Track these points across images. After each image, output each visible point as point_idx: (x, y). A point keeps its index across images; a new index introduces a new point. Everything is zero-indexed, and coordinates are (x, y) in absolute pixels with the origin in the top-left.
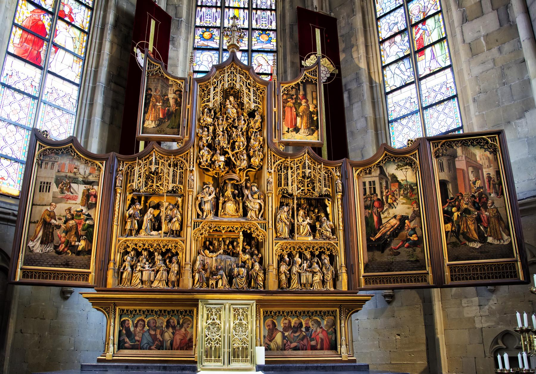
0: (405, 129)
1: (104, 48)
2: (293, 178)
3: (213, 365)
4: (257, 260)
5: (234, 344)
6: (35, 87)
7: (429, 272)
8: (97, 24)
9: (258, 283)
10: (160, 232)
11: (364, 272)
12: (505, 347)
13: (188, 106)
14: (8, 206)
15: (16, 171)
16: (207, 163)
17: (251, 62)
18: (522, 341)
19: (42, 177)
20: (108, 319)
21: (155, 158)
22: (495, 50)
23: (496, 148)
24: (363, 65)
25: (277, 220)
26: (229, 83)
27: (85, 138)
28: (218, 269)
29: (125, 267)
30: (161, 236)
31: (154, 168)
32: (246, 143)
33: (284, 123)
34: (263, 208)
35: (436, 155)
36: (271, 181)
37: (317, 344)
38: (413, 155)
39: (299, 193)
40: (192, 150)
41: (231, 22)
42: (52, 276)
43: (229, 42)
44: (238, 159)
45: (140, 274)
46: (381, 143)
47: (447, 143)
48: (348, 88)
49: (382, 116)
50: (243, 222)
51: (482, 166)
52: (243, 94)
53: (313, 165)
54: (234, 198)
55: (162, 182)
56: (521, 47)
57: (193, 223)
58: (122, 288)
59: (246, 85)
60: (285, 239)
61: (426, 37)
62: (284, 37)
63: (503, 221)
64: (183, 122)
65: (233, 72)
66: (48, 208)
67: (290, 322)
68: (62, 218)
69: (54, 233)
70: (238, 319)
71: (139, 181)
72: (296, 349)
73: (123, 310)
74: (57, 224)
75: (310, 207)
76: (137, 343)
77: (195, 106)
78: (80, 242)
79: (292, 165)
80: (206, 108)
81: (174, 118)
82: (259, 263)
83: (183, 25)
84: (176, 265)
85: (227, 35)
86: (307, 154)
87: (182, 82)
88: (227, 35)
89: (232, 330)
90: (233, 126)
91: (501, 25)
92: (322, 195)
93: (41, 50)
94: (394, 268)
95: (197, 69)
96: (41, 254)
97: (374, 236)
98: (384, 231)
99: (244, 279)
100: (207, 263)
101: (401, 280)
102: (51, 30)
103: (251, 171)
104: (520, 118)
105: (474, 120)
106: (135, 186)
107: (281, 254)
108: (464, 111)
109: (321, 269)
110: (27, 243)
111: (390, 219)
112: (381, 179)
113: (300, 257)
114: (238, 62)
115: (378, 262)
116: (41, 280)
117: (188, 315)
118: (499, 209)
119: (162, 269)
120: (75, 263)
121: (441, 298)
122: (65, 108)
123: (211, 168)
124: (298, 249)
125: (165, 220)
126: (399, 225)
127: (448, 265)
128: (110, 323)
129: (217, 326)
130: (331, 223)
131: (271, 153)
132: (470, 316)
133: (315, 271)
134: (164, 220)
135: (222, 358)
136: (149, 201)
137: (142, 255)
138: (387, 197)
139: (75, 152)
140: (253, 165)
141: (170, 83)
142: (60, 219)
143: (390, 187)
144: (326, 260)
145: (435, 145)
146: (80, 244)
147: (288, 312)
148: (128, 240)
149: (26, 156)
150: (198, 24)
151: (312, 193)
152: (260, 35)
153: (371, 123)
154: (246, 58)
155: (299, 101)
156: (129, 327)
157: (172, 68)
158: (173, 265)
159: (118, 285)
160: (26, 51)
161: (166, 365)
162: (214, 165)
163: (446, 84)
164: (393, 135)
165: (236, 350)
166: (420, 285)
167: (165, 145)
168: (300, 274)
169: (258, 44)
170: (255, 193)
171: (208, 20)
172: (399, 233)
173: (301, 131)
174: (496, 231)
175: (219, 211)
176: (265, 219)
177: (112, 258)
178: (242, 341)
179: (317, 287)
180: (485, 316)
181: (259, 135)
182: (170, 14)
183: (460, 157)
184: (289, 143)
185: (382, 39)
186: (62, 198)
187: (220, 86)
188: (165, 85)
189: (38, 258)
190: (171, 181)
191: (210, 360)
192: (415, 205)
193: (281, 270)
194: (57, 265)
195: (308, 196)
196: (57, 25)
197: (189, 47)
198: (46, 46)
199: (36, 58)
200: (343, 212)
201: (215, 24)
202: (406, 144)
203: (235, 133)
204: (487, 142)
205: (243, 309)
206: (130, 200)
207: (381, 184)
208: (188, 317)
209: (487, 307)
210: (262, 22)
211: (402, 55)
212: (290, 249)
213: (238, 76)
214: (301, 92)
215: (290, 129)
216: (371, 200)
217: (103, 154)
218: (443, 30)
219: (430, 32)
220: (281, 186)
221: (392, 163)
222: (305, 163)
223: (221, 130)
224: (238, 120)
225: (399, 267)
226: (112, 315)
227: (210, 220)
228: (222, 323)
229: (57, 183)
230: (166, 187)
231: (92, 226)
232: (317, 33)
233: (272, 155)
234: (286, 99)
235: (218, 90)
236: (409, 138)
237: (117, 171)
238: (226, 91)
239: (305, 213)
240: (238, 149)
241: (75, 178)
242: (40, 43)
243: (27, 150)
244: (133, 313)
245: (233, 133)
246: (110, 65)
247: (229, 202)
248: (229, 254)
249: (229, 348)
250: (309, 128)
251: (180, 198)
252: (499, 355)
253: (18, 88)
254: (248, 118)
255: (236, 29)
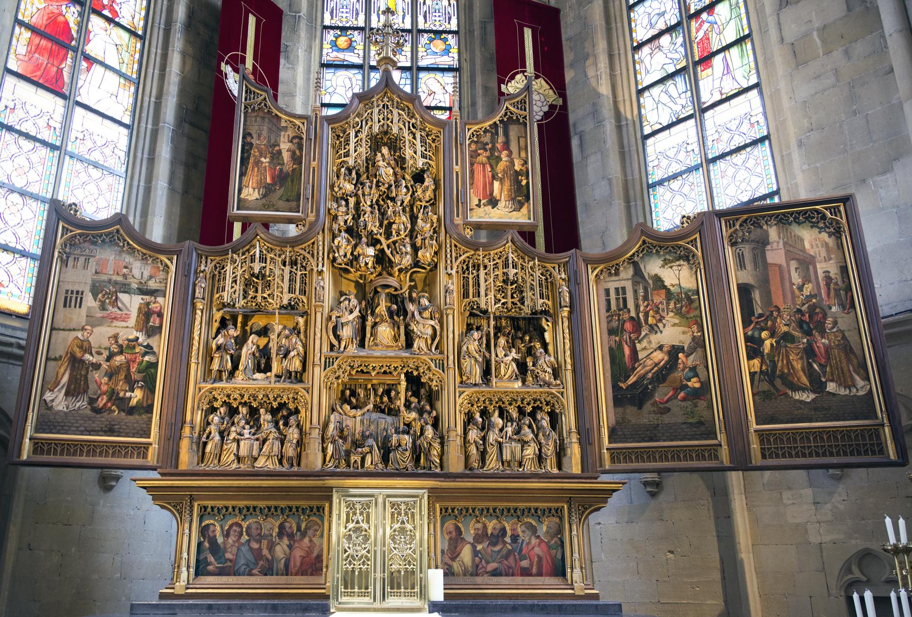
0: (678, 196)
1: (171, 63)
2: (487, 283)
3: (357, 601)
4: (430, 421)
5: (391, 565)
6: (55, 129)
7: (723, 443)
8: (158, 22)
9: (432, 459)
10: (269, 374)
11: (610, 442)
12: (865, 579)
13: (314, 164)
14: (9, 332)
15: (24, 271)
16: (345, 260)
17: (417, 89)
18: (898, 569)
19: (69, 282)
20: (179, 523)
21: (260, 251)
22: (838, 54)
23: (841, 227)
24: (604, 89)
25: (462, 354)
26: (381, 123)
27: (141, 217)
28: (364, 437)
29: (210, 433)
30: (270, 382)
31: (259, 268)
32: (409, 226)
33: (472, 190)
34: (438, 333)
35: (731, 240)
36: (451, 288)
37: (531, 564)
38: (692, 241)
39: (498, 309)
40: (320, 237)
41: (382, 18)
42: (85, 450)
43: (379, 54)
44: (397, 253)
45: (235, 445)
46: (635, 222)
47: (751, 220)
48: (578, 131)
49: (637, 176)
50: (406, 358)
51: (814, 258)
52: (405, 142)
53: (521, 261)
54: (391, 317)
55: (272, 290)
56: (886, 47)
57: (323, 360)
58: (204, 470)
59: (409, 127)
60: (475, 385)
61: (714, 35)
62: (470, 43)
63: (854, 354)
64: (306, 190)
65: (387, 105)
66: (79, 334)
67: (485, 527)
68: (103, 351)
69: (89, 376)
70: (398, 521)
71: (233, 290)
72: (495, 573)
73: (205, 508)
74: (94, 361)
75: (516, 332)
76: (229, 564)
77: (324, 163)
78: (133, 392)
79: (486, 261)
80: (343, 167)
81: (290, 184)
82: (433, 425)
83: (303, 25)
84: (296, 431)
85: (376, 41)
86: (510, 244)
87: (303, 123)
88: (376, 41)
89: (388, 540)
90: (388, 197)
91: (849, 9)
92: (536, 311)
93: (63, 66)
94: (660, 435)
95: (326, 100)
96: (65, 413)
97: (626, 381)
98: (642, 372)
99: (407, 453)
100: (347, 426)
101: (673, 457)
102: (79, 31)
103: (419, 272)
104: (885, 172)
105: (800, 179)
106: (226, 298)
107: (469, 411)
108: (781, 164)
109: (537, 436)
110: (42, 394)
111: (652, 352)
112: (635, 283)
113: (501, 416)
114: (396, 89)
115: (633, 425)
116: (65, 457)
117: (315, 514)
118: (847, 334)
119: (271, 437)
120: (125, 427)
121: (745, 488)
122: (106, 164)
123: (352, 267)
124: (497, 403)
125: (277, 354)
126: (667, 363)
127: (755, 431)
128: (183, 530)
129: (364, 533)
130: (552, 359)
131: (451, 242)
132: (798, 521)
133: (526, 439)
134: (275, 355)
135: (371, 589)
136: (250, 324)
137: (239, 413)
138: (646, 315)
139: (125, 240)
140: (422, 262)
141: (283, 124)
142: (99, 353)
143: (652, 296)
144: (544, 421)
145: (730, 224)
146: (133, 395)
147: (482, 509)
148: (215, 389)
149: (41, 246)
150: (327, 22)
151: (520, 309)
152: (431, 40)
153: (618, 189)
154: (409, 82)
155: (496, 154)
156: (215, 536)
157: (286, 98)
158: (291, 429)
159: (198, 464)
160: (38, 67)
161: (276, 602)
162: (358, 263)
163: (749, 117)
164: (655, 208)
165: (395, 574)
166: (707, 465)
167: (276, 229)
168: (500, 444)
169: (428, 57)
170: (426, 309)
171: (344, 15)
172: (667, 375)
173: (501, 204)
174: (843, 373)
175: (367, 340)
176: (442, 353)
177: (188, 418)
178: (405, 560)
179: (529, 467)
180: (826, 522)
181: (431, 211)
182: (280, 6)
183: (775, 244)
184: (481, 225)
185: (638, 42)
186: (103, 317)
187: (366, 129)
188: (274, 128)
189: (60, 420)
190: (286, 290)
191: (351, 592)
192: (695, 328)
193: (470, 438)
194: (95, 431)
195: (513, 314)
196: (90, 24)
197: (312, 63)
198: (72, 59)
199: (54, 80)
200: (572, 340)
201: (355, 22)
202: (678, 223)
203: (391, 208)
204: (824, 217)
205: (406, 504)
206: (219, 320)
207: (635, 292)
208: (315, 518)
209: (829, 506)
210: (434, 18)
211: (671, 69)
212: (484, 402)
213: (395, 111)
214: (501, 139)
215: (483, 202)
216: (619, 319)
217: (173, 244)
218: (745, 22)
219: (721, 27)
220: (468, 297)
221: (655, 257)
222: (507, 258)
223: (369, 203)
224: (395, 187)
225: (669, 434)
226: (187, 517)
227: (351, 354)
228: (372, 528)
229: (95, 292)
230: (279, 299)
231: (155, 365)
232: (526, 36)
233: (453, 245)
234: (476, 151)
235: (363, 135)
236: (684, 213)
237: (196, 272)
238: (376, 137)
239: (507, 342)
240: (397, 236)
241: (125, 285)
242: (61, 56)
243: (42, 236)
244: (222, 513)
245: (389, 208)
246: (182, 92)
247: (383, 324)
248: (382, 411)
249: (384, 572)
250: (513, 199)
251: (302, 317)
252: (855, 593)
253: (25, 131)
254: (412, 183)
255: (391, 32)
